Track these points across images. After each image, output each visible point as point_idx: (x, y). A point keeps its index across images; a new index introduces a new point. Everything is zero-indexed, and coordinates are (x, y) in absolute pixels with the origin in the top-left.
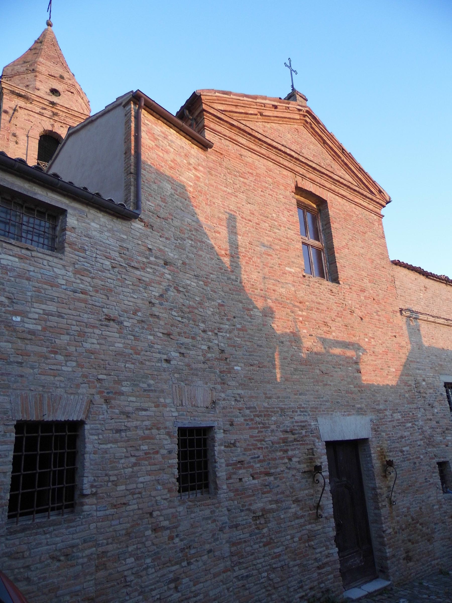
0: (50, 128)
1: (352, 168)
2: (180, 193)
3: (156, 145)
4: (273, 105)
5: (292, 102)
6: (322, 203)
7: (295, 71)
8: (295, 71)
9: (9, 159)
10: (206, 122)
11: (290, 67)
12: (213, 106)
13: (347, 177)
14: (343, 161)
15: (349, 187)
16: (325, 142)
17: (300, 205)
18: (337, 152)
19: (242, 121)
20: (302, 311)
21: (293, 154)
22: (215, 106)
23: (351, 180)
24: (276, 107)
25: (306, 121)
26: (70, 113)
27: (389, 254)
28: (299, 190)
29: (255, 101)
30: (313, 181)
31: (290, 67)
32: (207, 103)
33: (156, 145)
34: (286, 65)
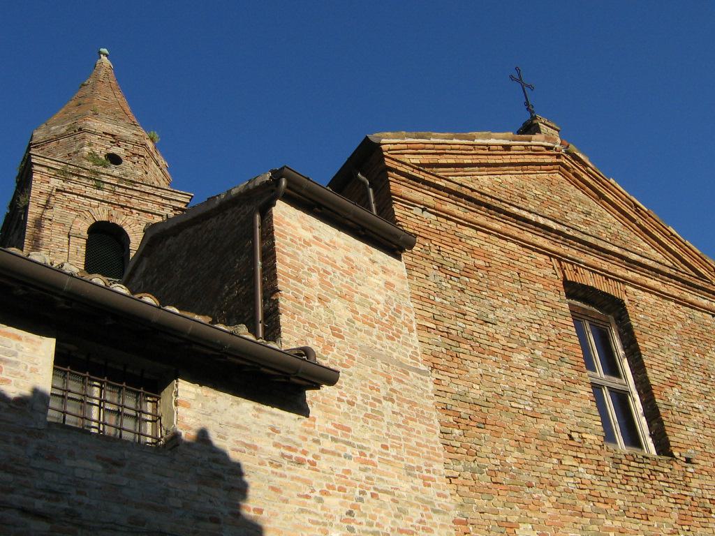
0: (104, 218)
1: (658, 236)
2: (364, 316)
3: (314, 237)
4: (503, 146)
5: (534, 137)
6: (615, 308)
7: (528, 86)
8: (528, 86)
9: (116, 294)
10: (394, 187)
11: (520, 80)
12: (403, 160)
13: (659, 257)
14: (639, 226)
15: (658, 271)
16: (601, 196)
17: (577, 316)
18: (628, 211)
19: (454, 179)
20: (613, 518)
21: (551, 224)
22: (405, 158)
23: (659, 257)
24: (507, 148)
25: (562, 164)
26: (138, 189)
27: (15, 189)
28: (573, 290)
29: (472, 142)
30: (593, 269)
31: (520, 80)
32: (392, 156)
33: (314, 237)
34: (531, 88)
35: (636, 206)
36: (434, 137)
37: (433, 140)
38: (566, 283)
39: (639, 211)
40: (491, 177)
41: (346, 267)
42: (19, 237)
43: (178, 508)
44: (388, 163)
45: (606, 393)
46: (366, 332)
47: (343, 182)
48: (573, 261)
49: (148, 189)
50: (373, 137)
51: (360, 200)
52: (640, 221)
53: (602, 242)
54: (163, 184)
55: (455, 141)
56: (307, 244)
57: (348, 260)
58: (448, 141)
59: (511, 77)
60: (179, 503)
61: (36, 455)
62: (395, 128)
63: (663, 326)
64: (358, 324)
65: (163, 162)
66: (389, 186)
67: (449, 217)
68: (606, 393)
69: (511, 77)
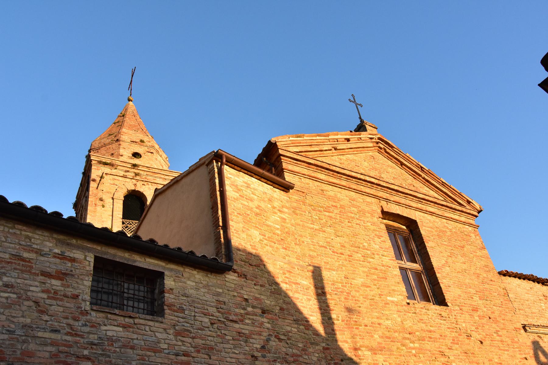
0: (133, 188)
2: (268, 237)
3: (240, 195)
6: (412, 224)
7: (359, 105)
8: (359, 105)
10: (284, 165)
12: (289, 150)
14: (424, 178)
16: (402, 164)
19: (317, 159)
20: (413, 342)
24: (348, 140)
29: (327, 138)
30: (398, 203)
31: (354, 102)
35: (422, 167)
36: (307, 136)
37: (305, 138)
38: (383, 212)
39: (423, 171)
40: (339, 156)
41: (258, 211)
42: (86, 200)
43: (165, 349)
44: (281, 152)
45: (409, 273)
46: (271, 246)
47: (259, 162)
48: (387, 200)
49: (156, 171)
50: (273, 140)
51: (269, 164)
52: (423, 175)
53: (327, 149)
54: (166, 168)
55: (318, 138)
56: (237, 199)
57: (258, 207)
58: (314, 138)
59: (349, 100)
60: (166, 346)
61: (86, 325)
62: (283, 134)
63: (441, 233)
64: (265, 242)
65: (164, 156)
66: (281, 159)
67: (316, 179)
68: (409, 273)
69: (349, 100)
